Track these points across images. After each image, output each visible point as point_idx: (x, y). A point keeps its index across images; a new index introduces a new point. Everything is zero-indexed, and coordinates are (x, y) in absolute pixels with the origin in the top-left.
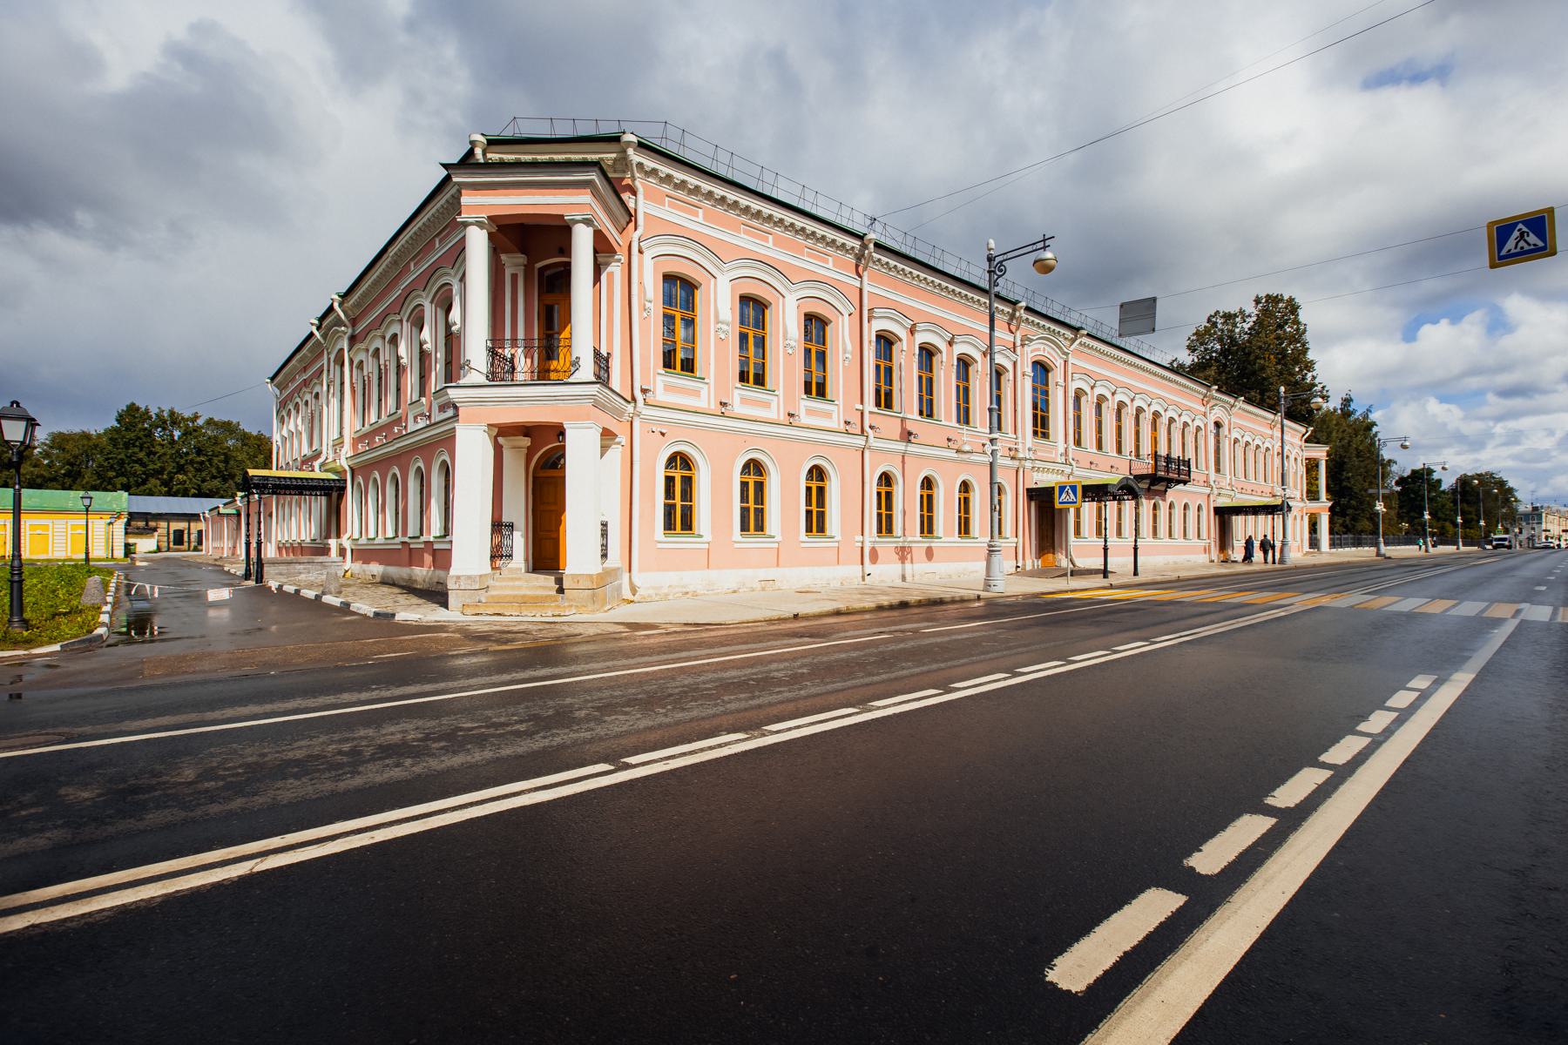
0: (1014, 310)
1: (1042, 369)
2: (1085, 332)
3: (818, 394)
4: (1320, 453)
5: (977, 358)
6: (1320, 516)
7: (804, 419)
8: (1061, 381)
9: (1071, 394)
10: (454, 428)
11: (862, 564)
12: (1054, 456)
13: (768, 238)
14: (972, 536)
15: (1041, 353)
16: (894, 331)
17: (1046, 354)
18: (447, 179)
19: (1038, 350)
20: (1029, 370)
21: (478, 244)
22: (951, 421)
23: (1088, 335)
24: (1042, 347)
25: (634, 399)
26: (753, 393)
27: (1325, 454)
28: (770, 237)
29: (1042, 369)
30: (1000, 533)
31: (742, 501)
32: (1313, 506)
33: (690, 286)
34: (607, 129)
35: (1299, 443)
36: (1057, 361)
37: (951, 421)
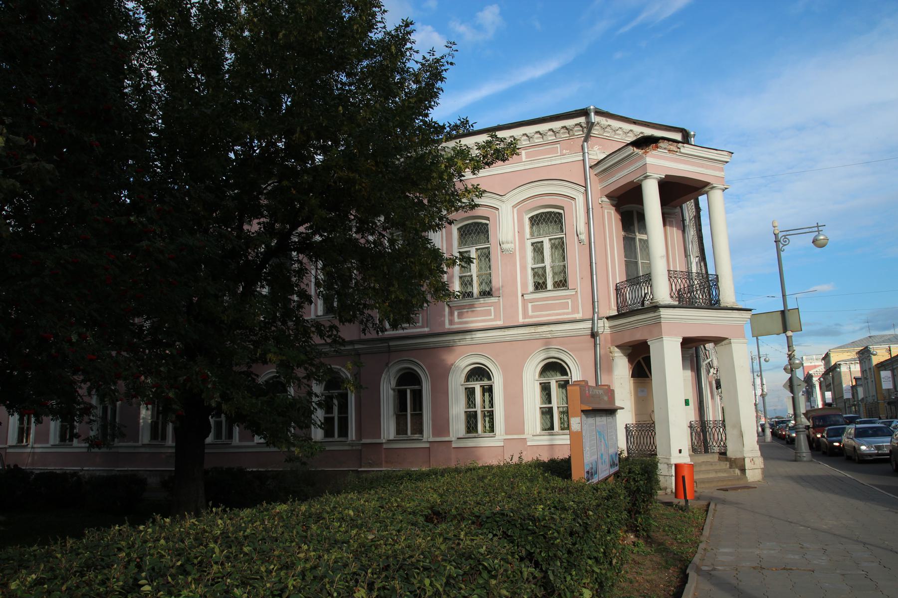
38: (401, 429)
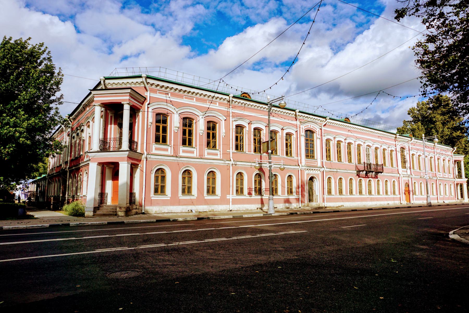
0: (396, 136)
1: (310, 133)
2: (329, 118)
3: (163, 142)
4: (461, 158)
5: (293, 133)
6: (463, 184)
7: (182, 154)
8: (319, 137)
9: (324, 141)
10: (89, 163)
11: (438, 200)
12: (316, 164)
13: (216, 103)
14: (332, 194)
15: (309, 127)
16: (245, 125)
17: (311, 127)
18: (90, 93)
19: (308, 126)
20: (303, 133)
21: (98, 111)
22: (346, 162)
23: (330, 119)
24: (309, 125)
25: (299, 165)
26: (187, 149)
27: (463, 159)
28: (195, 98)
29: (310, 133)
30: (440, 194)
31: (255, 185)
32: (459, 181)
33: (191, 120)
34: (294, 108)
35: (451, 154)
36: (316, 129)
37: (346, 162)
38: (210, 133)
